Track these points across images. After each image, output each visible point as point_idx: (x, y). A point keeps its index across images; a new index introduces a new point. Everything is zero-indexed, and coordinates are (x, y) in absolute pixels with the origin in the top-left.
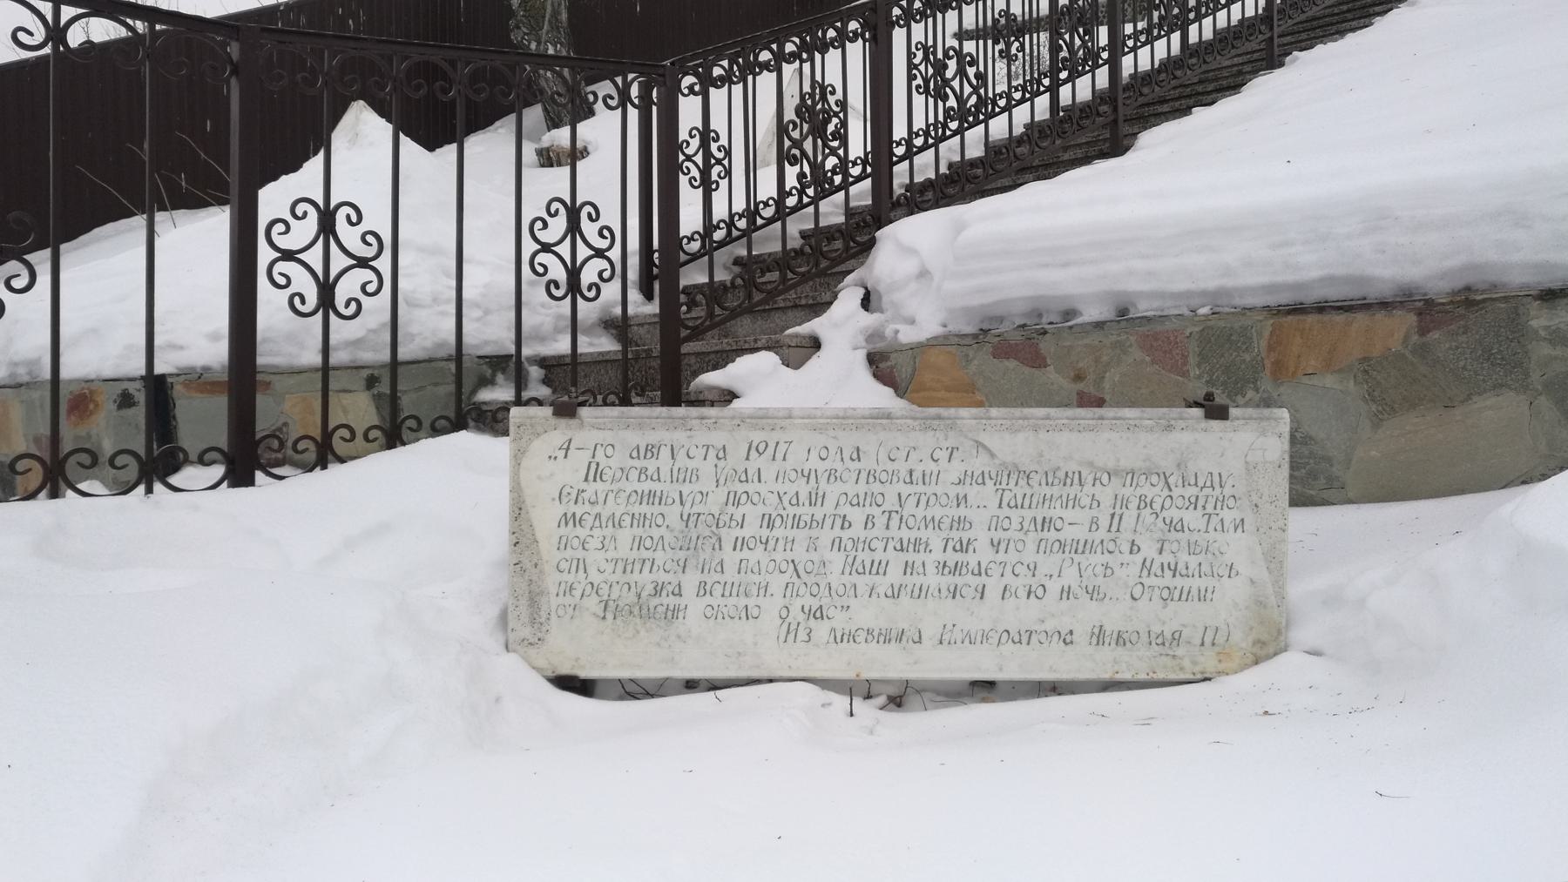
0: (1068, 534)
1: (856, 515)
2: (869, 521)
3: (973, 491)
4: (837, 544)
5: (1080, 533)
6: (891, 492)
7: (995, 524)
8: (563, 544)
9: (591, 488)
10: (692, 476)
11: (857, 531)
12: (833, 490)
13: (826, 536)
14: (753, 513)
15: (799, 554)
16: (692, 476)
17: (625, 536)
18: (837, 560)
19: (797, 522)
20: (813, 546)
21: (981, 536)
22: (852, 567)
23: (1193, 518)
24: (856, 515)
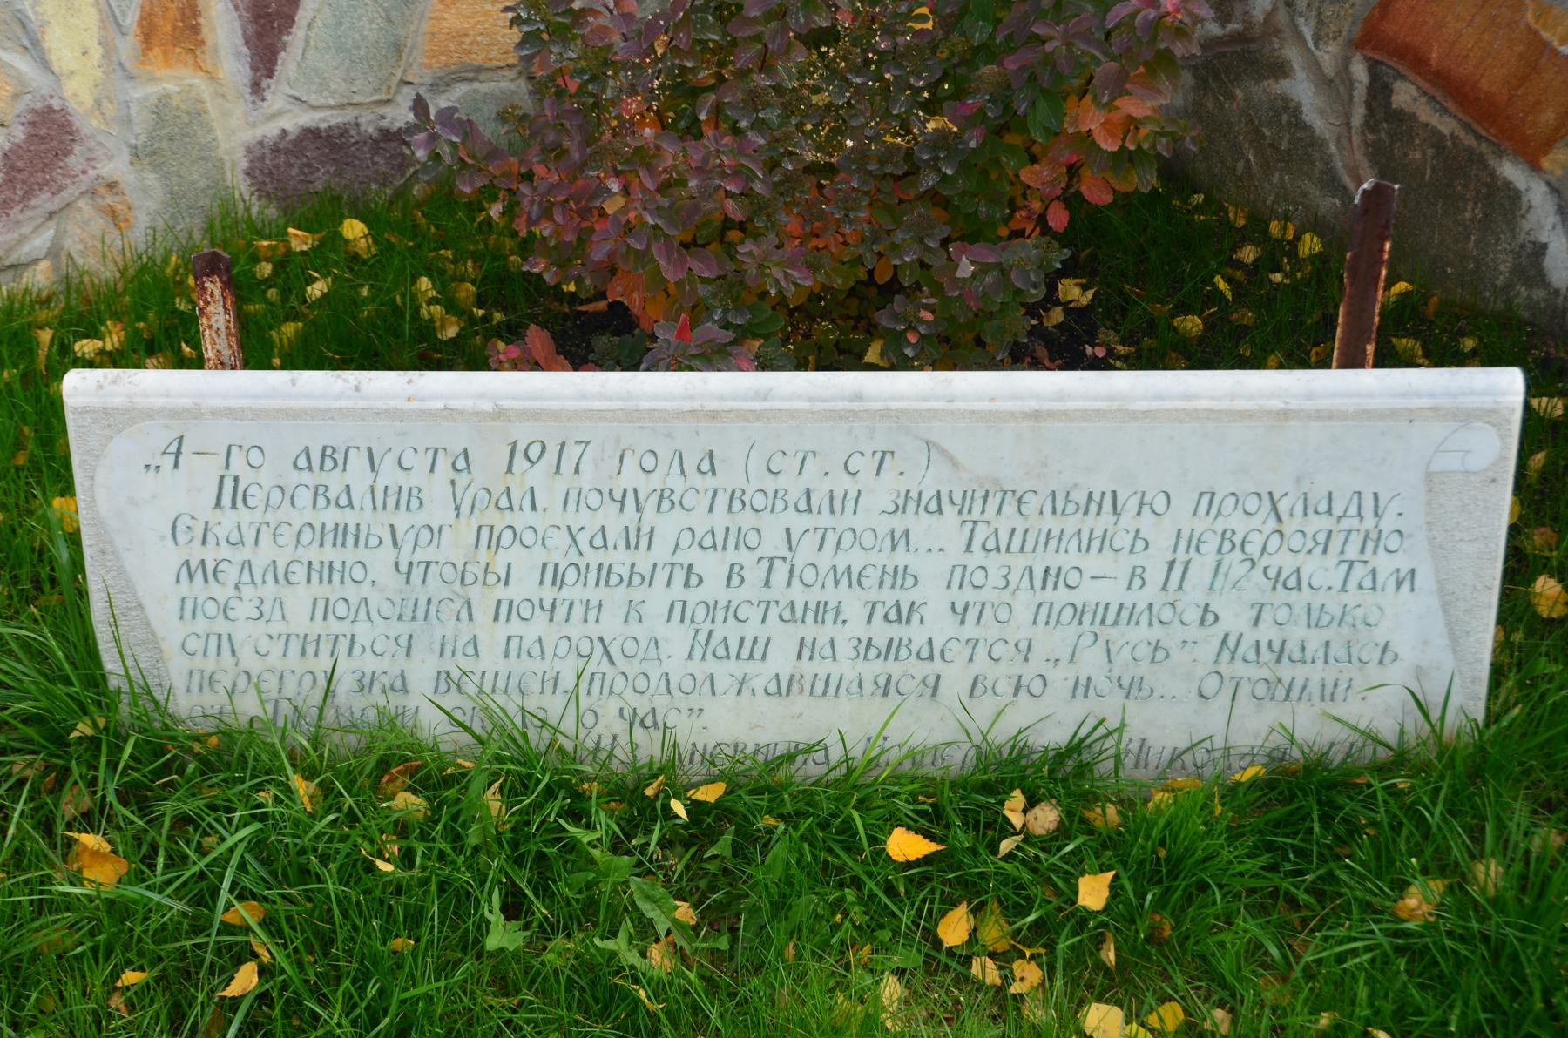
0: (1089, 593)
1: (712, 566)
2: (733, 575)
3: (920, 525)
4: (679, 611)
5: (1111, 592)
6: (773, 528)
7: (959, 577)
8: (189, 610)
9: (227, 521)
10: (409, 499)
11: (714, 589)
12: (668, 525)
13: (657, 599)
14: (524, 563)
15: (611, 625)
16: (409, 499)
17: (299, 598)
18: (677, 639)
19: (604, 574)
20: (633, 613)
21: (933, 596)
22: (706, 646)
23: (1321, 570)
24: (712, 566)
